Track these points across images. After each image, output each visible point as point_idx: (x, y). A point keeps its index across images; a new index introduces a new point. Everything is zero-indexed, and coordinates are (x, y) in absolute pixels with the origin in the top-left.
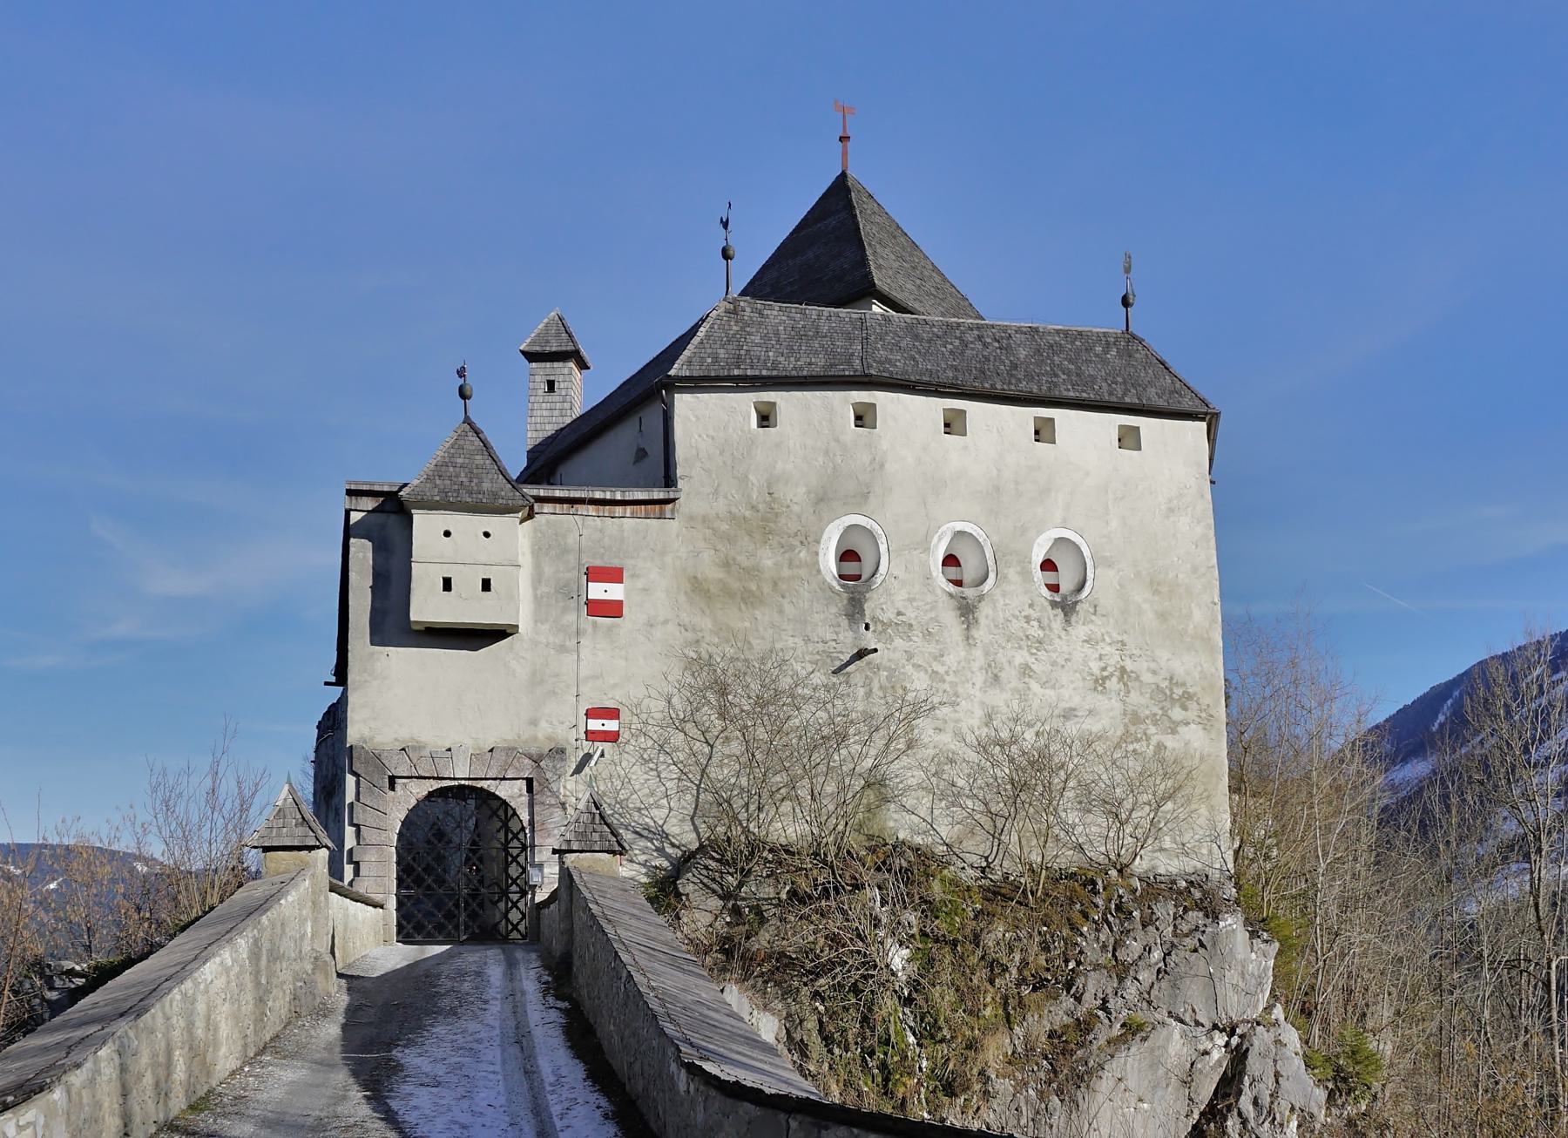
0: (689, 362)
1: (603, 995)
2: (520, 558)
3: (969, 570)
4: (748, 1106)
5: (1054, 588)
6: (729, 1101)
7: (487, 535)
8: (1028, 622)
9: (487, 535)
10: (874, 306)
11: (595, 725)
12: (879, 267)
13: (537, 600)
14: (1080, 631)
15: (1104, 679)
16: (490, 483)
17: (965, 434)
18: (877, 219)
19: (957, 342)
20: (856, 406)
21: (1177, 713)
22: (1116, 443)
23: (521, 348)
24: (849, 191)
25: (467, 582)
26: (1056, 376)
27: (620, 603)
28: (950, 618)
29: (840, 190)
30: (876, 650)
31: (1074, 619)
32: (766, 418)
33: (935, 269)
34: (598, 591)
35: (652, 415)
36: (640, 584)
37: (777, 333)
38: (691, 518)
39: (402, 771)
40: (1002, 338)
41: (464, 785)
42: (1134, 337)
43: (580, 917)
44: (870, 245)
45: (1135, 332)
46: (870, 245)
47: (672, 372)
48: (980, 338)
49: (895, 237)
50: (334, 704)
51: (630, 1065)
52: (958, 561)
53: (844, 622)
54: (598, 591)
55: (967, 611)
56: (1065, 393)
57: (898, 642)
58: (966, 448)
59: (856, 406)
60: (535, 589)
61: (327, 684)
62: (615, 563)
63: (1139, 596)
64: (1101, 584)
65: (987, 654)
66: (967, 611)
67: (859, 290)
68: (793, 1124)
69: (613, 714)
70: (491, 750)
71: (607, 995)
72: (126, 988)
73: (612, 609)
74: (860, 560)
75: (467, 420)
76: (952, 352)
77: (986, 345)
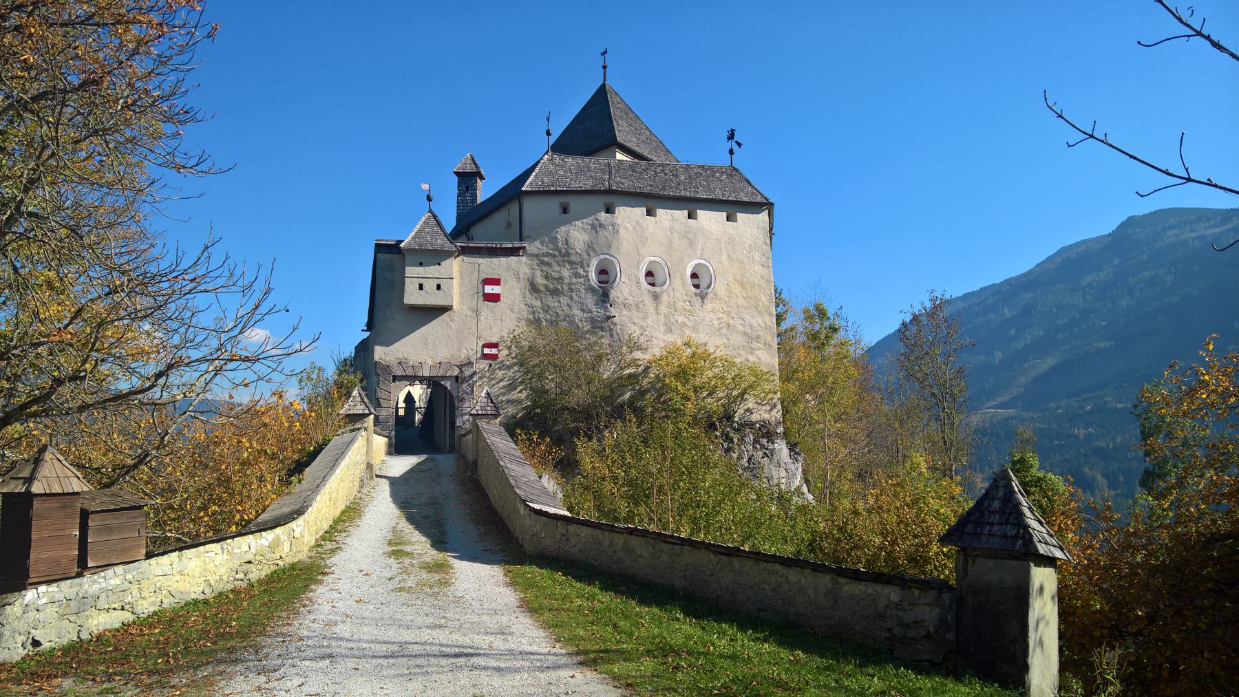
0: (531, 184)
1: (491, 478)
2: (454, 274)
3: (659, 278)
4: (544, 517)
5: (697, 286)
6: (538, 516)
8: (684, 303)
10: (617, 153)
11: (487, 351)
12: (619, 131)
13: (461, 294)
14: (709, 306)
15: (720, 328)
16: (442, 242)
17: (656, 216)
18: (620, 106)
19: (653, 173)
21: (755, 345)
22: (725, 219)
23: (455, 170)
24: (606, 93)
25: (430, 285)
26: (698, 188)
27: (499, 295)
28: (648, 300)
29: (601, 97)
30: (615, 316)
31: (706, 301)
33: (647, 128)
34: (489, 289)
35: (514, 207)
37: (570, 169)
40: (673, 170)
42: (735, 169)
43: (482, 443)
44: (615, 119)
45: (735, 167)
46: (615, 119)
47: (523, 189)
48: (663, 170)
49: (627, 114)
50: (365, 339)
51: (503, 507)
54: (489, 289)
55: (656, 297)
56: (702, 196)
57: (625, 312)
58: (656, 222)
60: (460, 289)
61: (363, 330)
63: (737, 289)
64: (719, 287)
65: (666, 317)
66: (656, 297)
67: (612, 143)
68: (559, 524)
69: (495, 345)
70: (440, 363)
71: (493, 479)
73: (495, 298)
74: (608, 274)
75: (430, 211)
76: (650, 178)
77: (666, 174)
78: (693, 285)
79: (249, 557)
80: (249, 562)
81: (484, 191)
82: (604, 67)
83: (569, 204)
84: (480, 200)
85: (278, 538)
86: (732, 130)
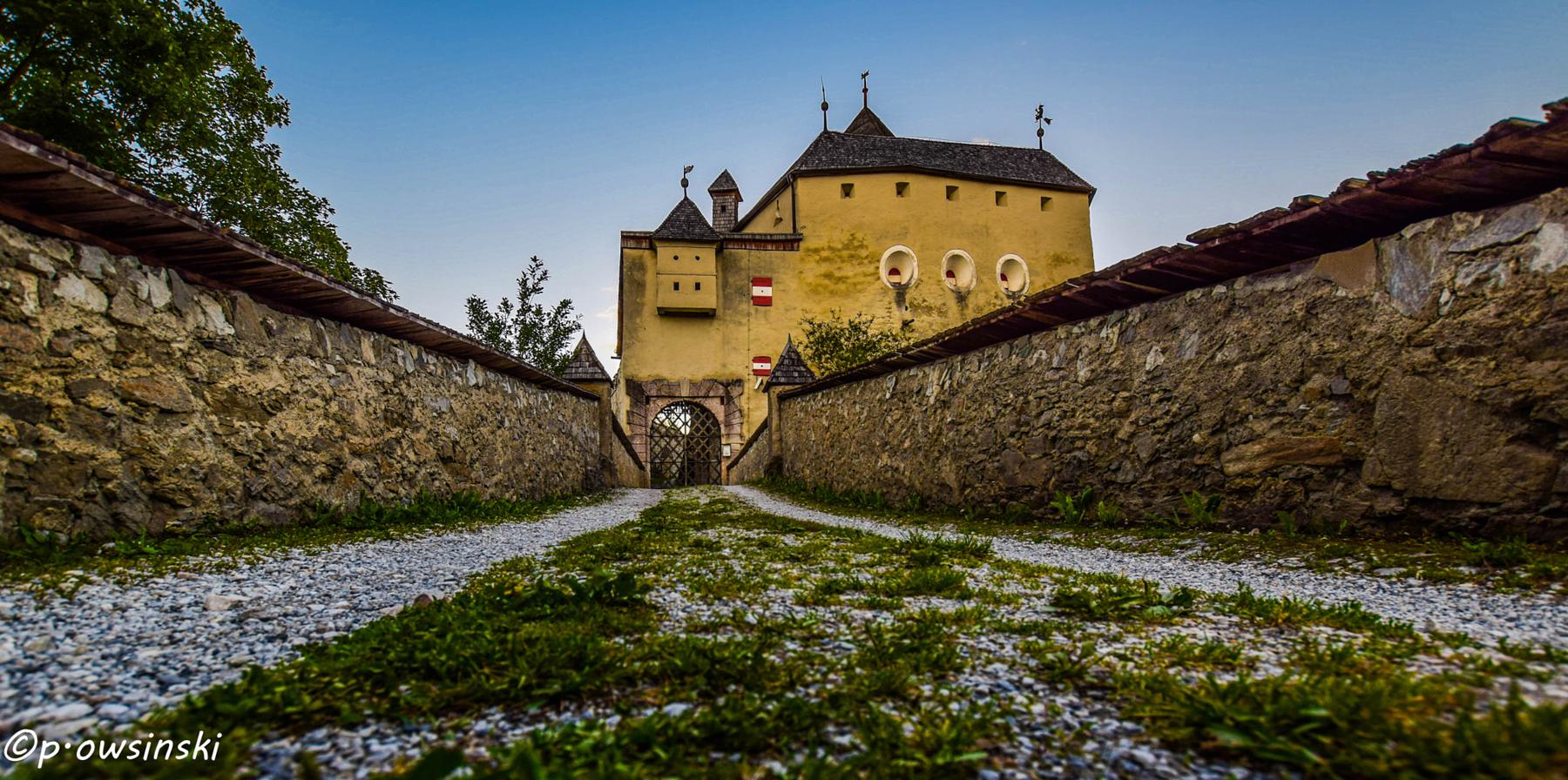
7: (698, 258)
9: (698, 258)
20: (844, 186)
32: (847, 190)
34: (758, 291)
36: (781, 287)
39: (654, 393)
41: (1287, 225)
53: (894, 306)
54: (758, 291)
59: (844, 186)
62: (769, 275)
73: (765, 302)
82: (865, 90)
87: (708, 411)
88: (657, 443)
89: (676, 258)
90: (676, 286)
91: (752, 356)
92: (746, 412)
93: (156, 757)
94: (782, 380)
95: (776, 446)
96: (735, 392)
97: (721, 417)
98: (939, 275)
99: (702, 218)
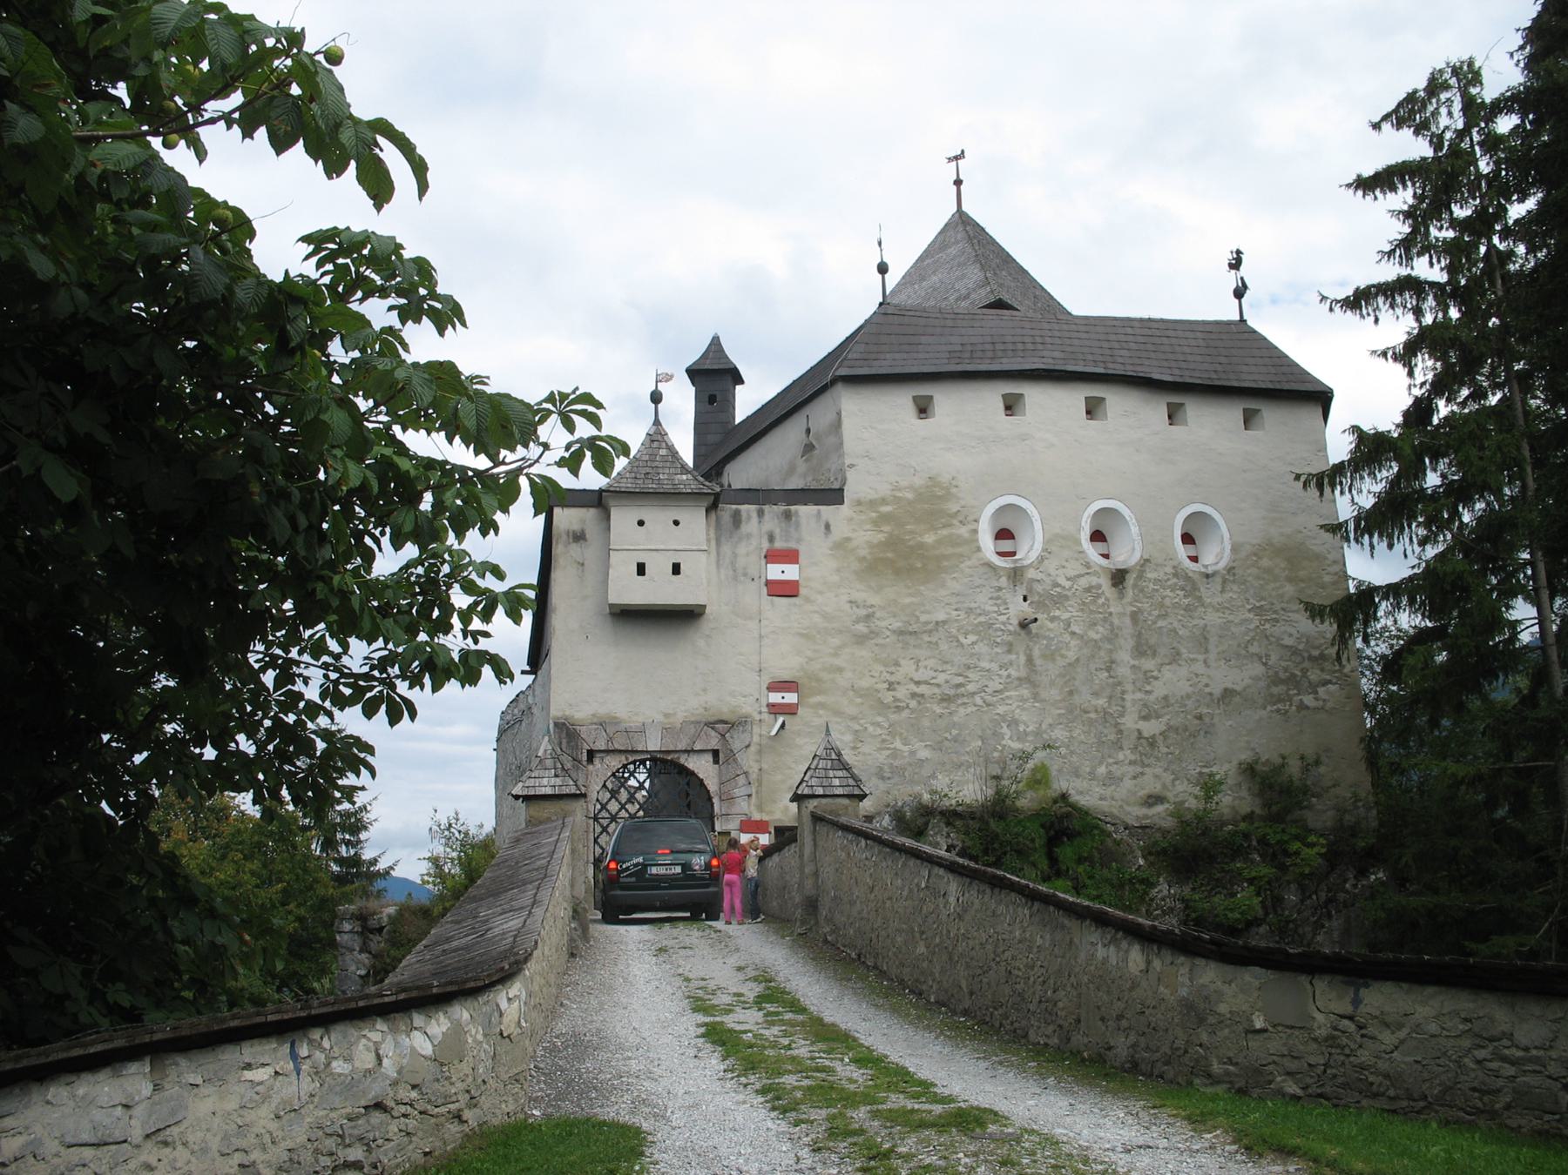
7: (676, 523)
9: (676, 523)
11: (775, 698)
25: (659, 566)
34: (776, 572)
38: (859, 503)
52: (1104, 537)
54: (776, 572)
62: (792, 545)
72: (404, 990)
78: (1189, 557)
79: (375, 1091)
80: (379, 1106)
81: (747, 401)
82: (958, 183)
83: (931, 398)
84: (738, 421)
85: (457, 1031)
86: (1239, 252)
87: (692, 774)
88: (605, 829)
89: (641, 523)
90: (641, 569)
91: (766, 681)
92: (753, 777)
93: (688, 914)
94: (820, 791)
95: (809, 883)
96: (737, 742)
97: (712, 786)
98: (1078, 542)
99: (674, 454)
